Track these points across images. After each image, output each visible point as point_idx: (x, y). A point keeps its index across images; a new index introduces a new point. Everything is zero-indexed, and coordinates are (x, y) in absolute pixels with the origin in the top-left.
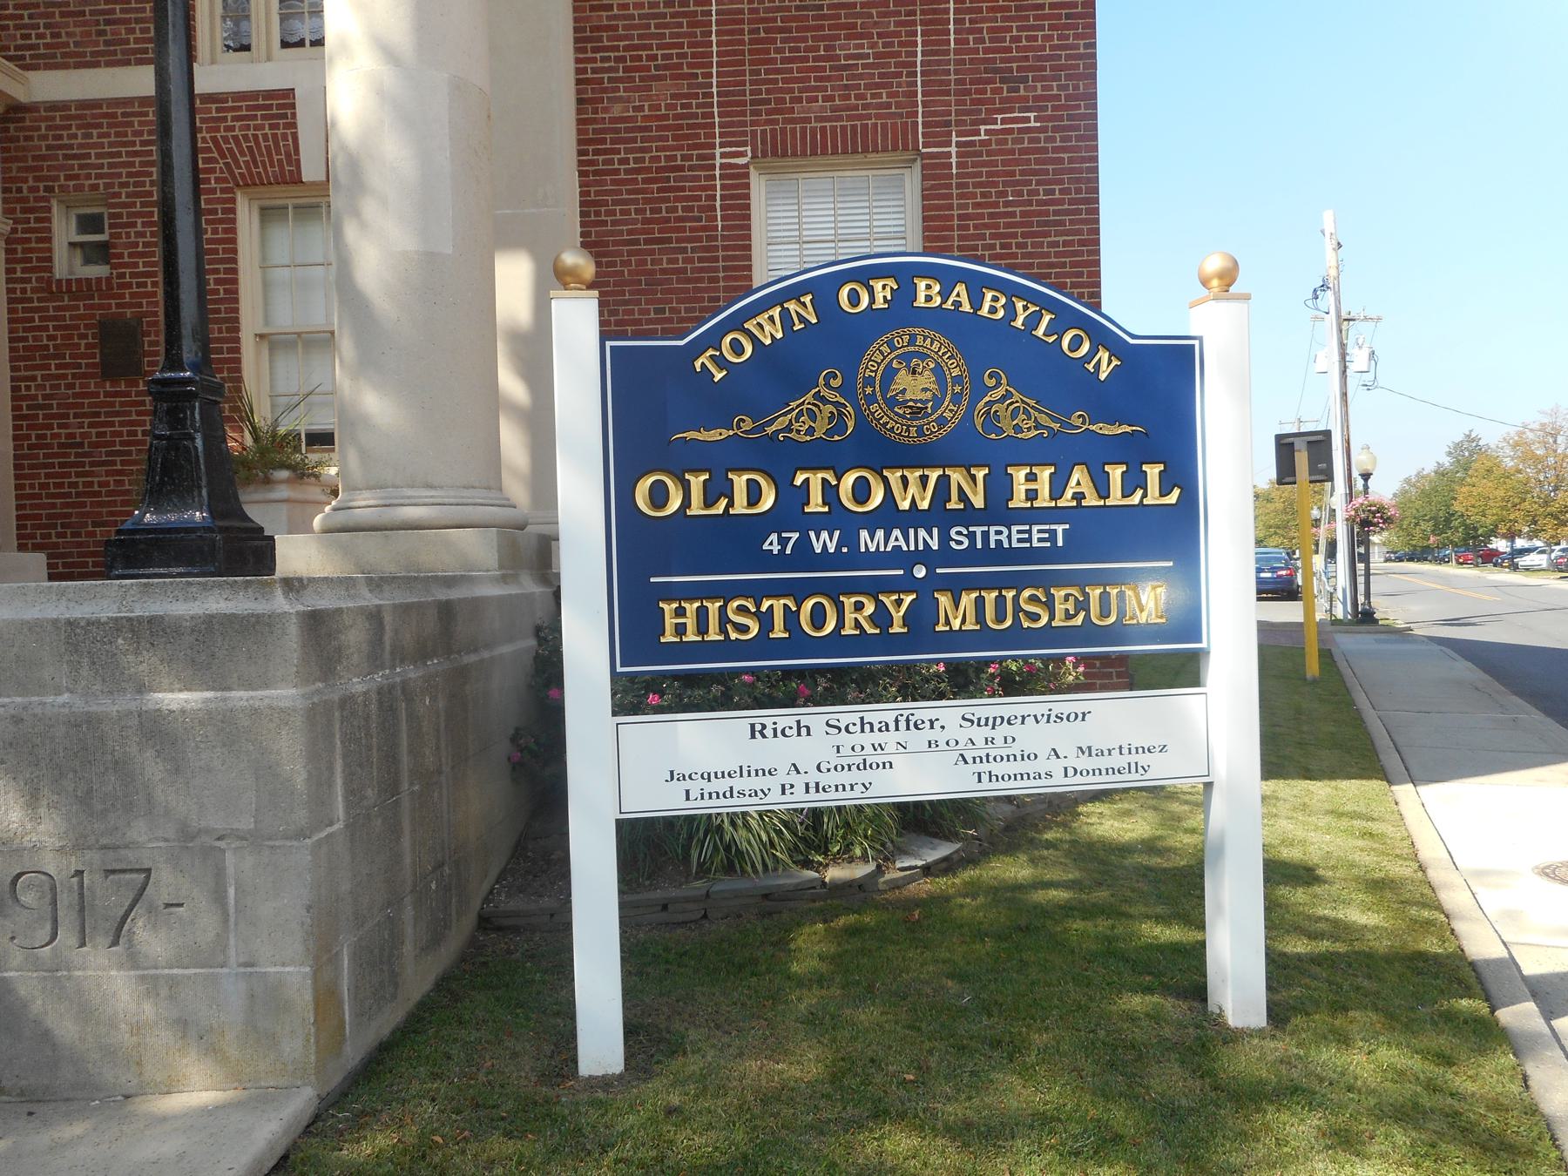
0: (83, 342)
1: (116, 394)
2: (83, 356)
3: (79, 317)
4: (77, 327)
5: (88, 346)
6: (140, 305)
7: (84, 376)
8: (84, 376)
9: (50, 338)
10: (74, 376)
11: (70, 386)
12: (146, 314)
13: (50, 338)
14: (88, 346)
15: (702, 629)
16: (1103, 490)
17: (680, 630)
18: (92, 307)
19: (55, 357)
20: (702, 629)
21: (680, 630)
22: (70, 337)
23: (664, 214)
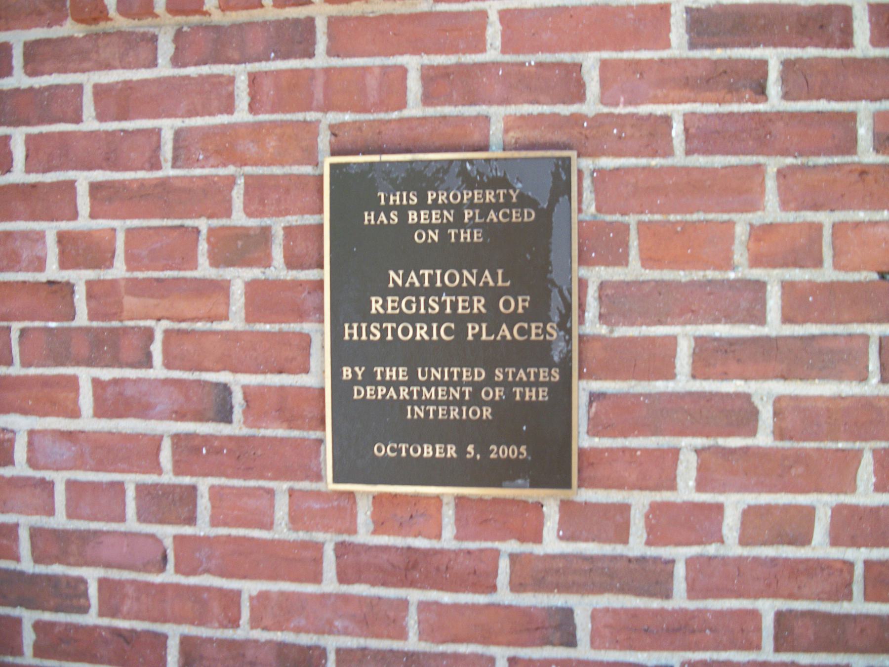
0: (239, 278)
1: (412, 568)
2: (237, 353)
3: (224, 145)
4: (213, 197)
5: (264, 300)
6: (571, 85)
7: (241, 456)
8: (241, 456)
9: (75, 251)
10: (189, 452)
11: (173, 504)
12: (592, 136)
13: (75, 251)
14: (264, 300)
15: (360, 334)
16: (495, 280)
17: (351, 335)
18: (294, 91)
19: (103, 347)
20: (360, 334)
21: (351, 335)
22: (181, 247)
23: (775, 100)
